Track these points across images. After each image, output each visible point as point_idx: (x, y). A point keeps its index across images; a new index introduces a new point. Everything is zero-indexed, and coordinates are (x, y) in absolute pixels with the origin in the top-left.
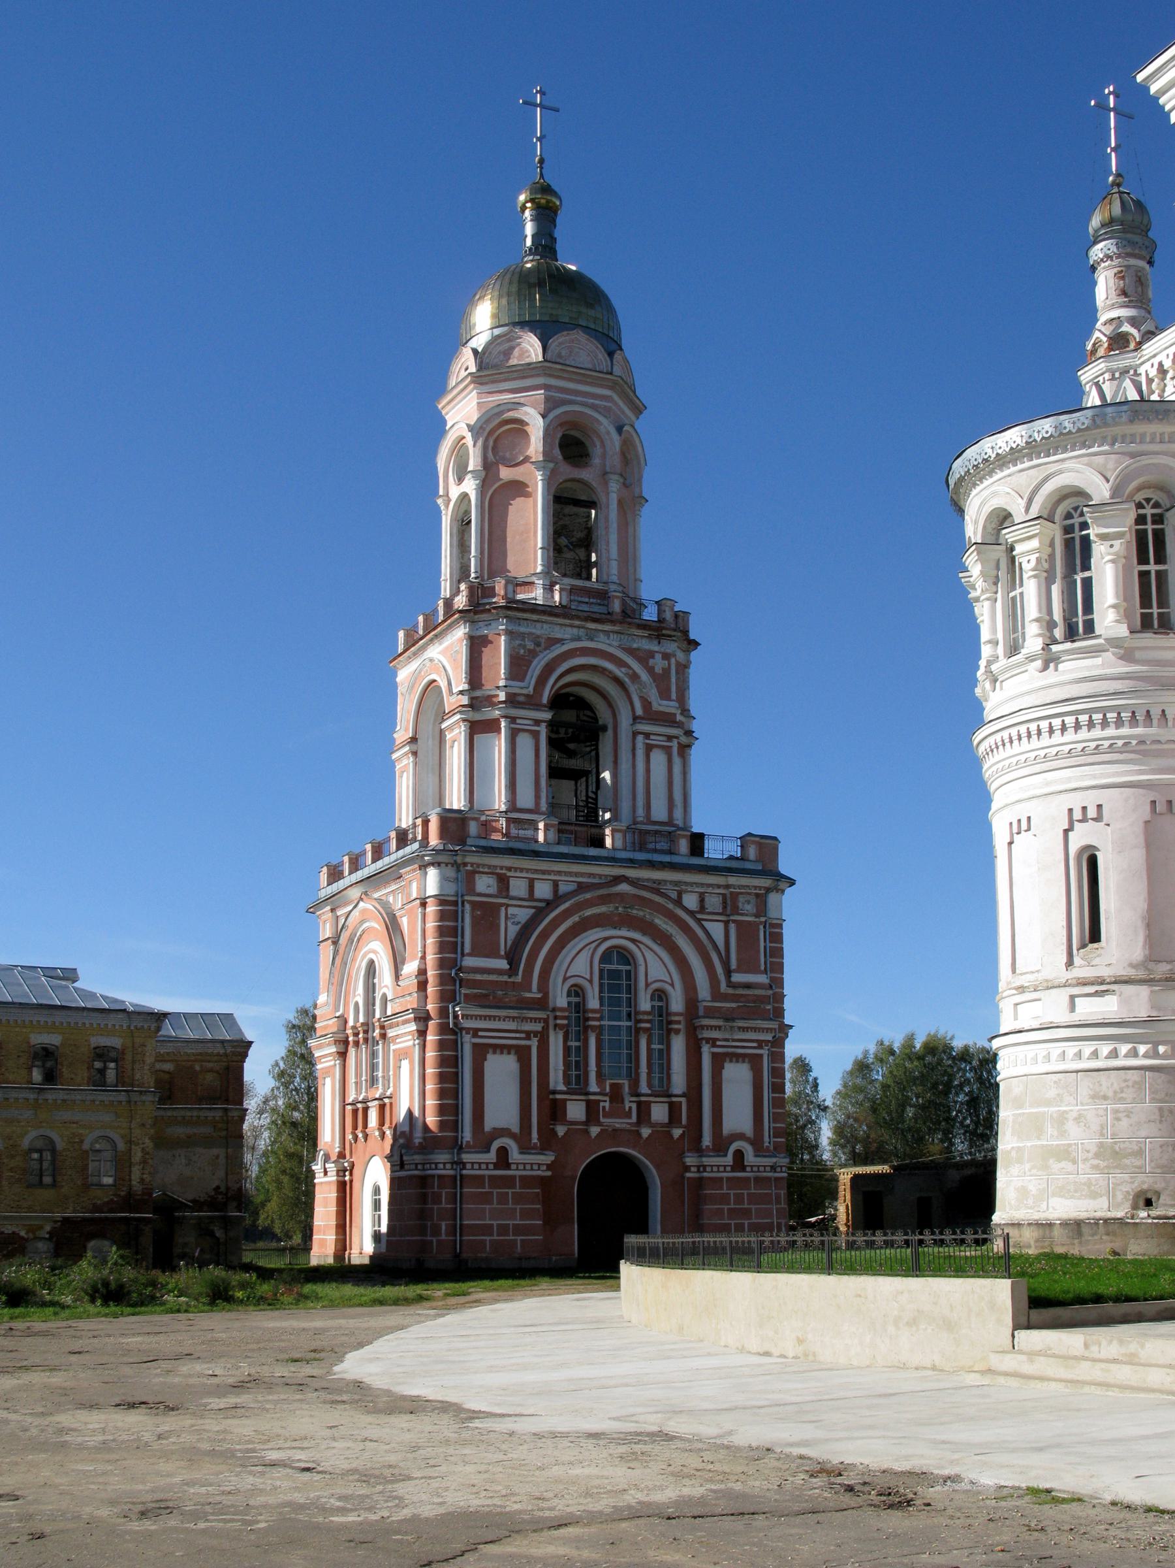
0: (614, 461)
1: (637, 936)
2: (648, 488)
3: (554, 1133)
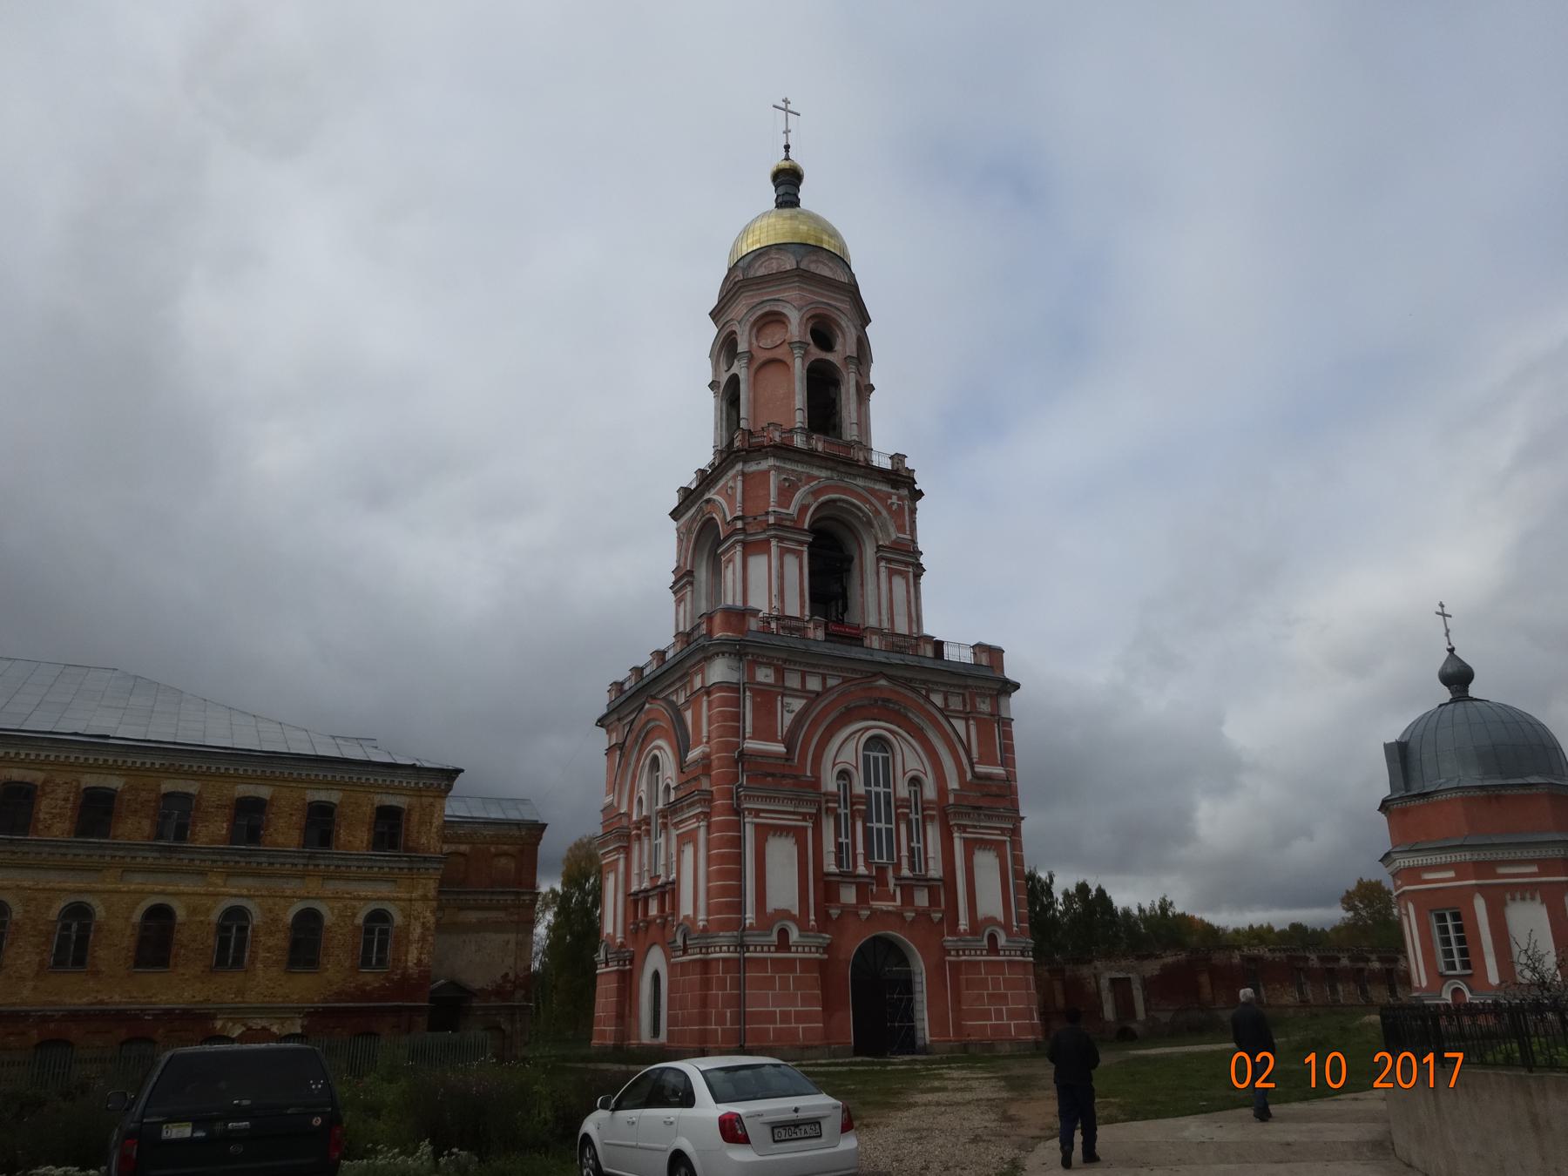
0: (851, 350)
2: (875, 377)
3: (828, 916)
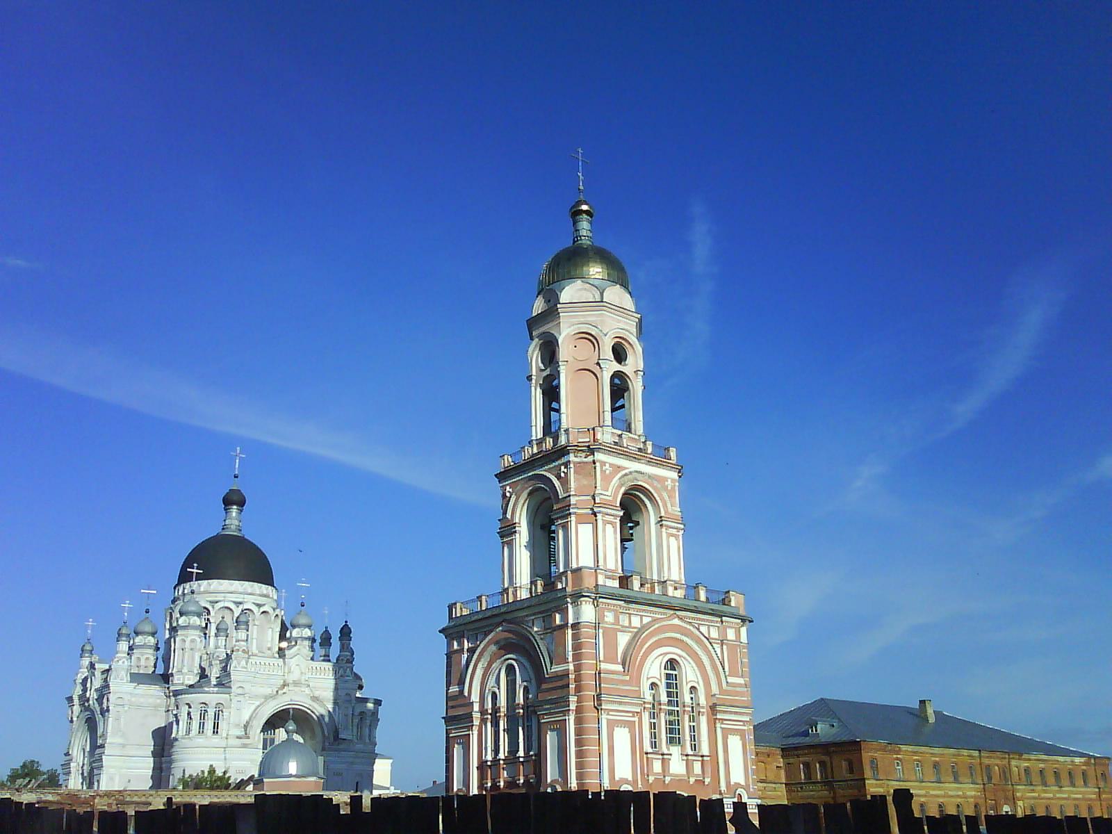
1: (684, 654)
